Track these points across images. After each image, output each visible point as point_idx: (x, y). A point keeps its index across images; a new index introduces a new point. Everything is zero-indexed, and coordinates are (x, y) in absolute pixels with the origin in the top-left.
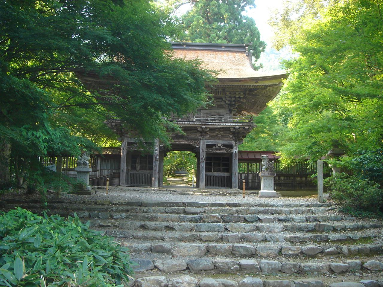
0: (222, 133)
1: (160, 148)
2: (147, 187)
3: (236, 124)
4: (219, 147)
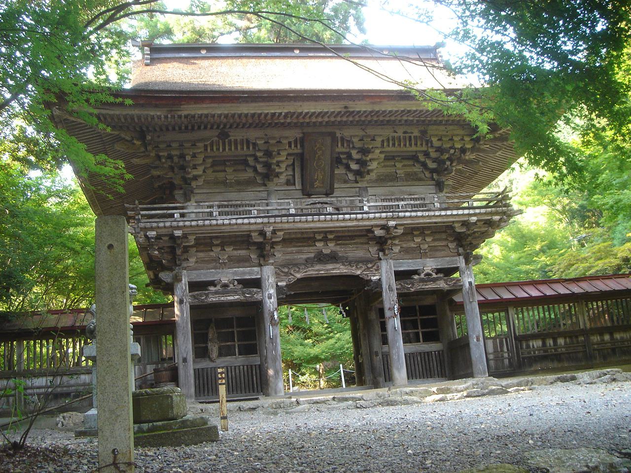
0: (429, 239)
1: (279, 289)
2: (257, 399)
3: (472, 211)
4: (428, 274)
